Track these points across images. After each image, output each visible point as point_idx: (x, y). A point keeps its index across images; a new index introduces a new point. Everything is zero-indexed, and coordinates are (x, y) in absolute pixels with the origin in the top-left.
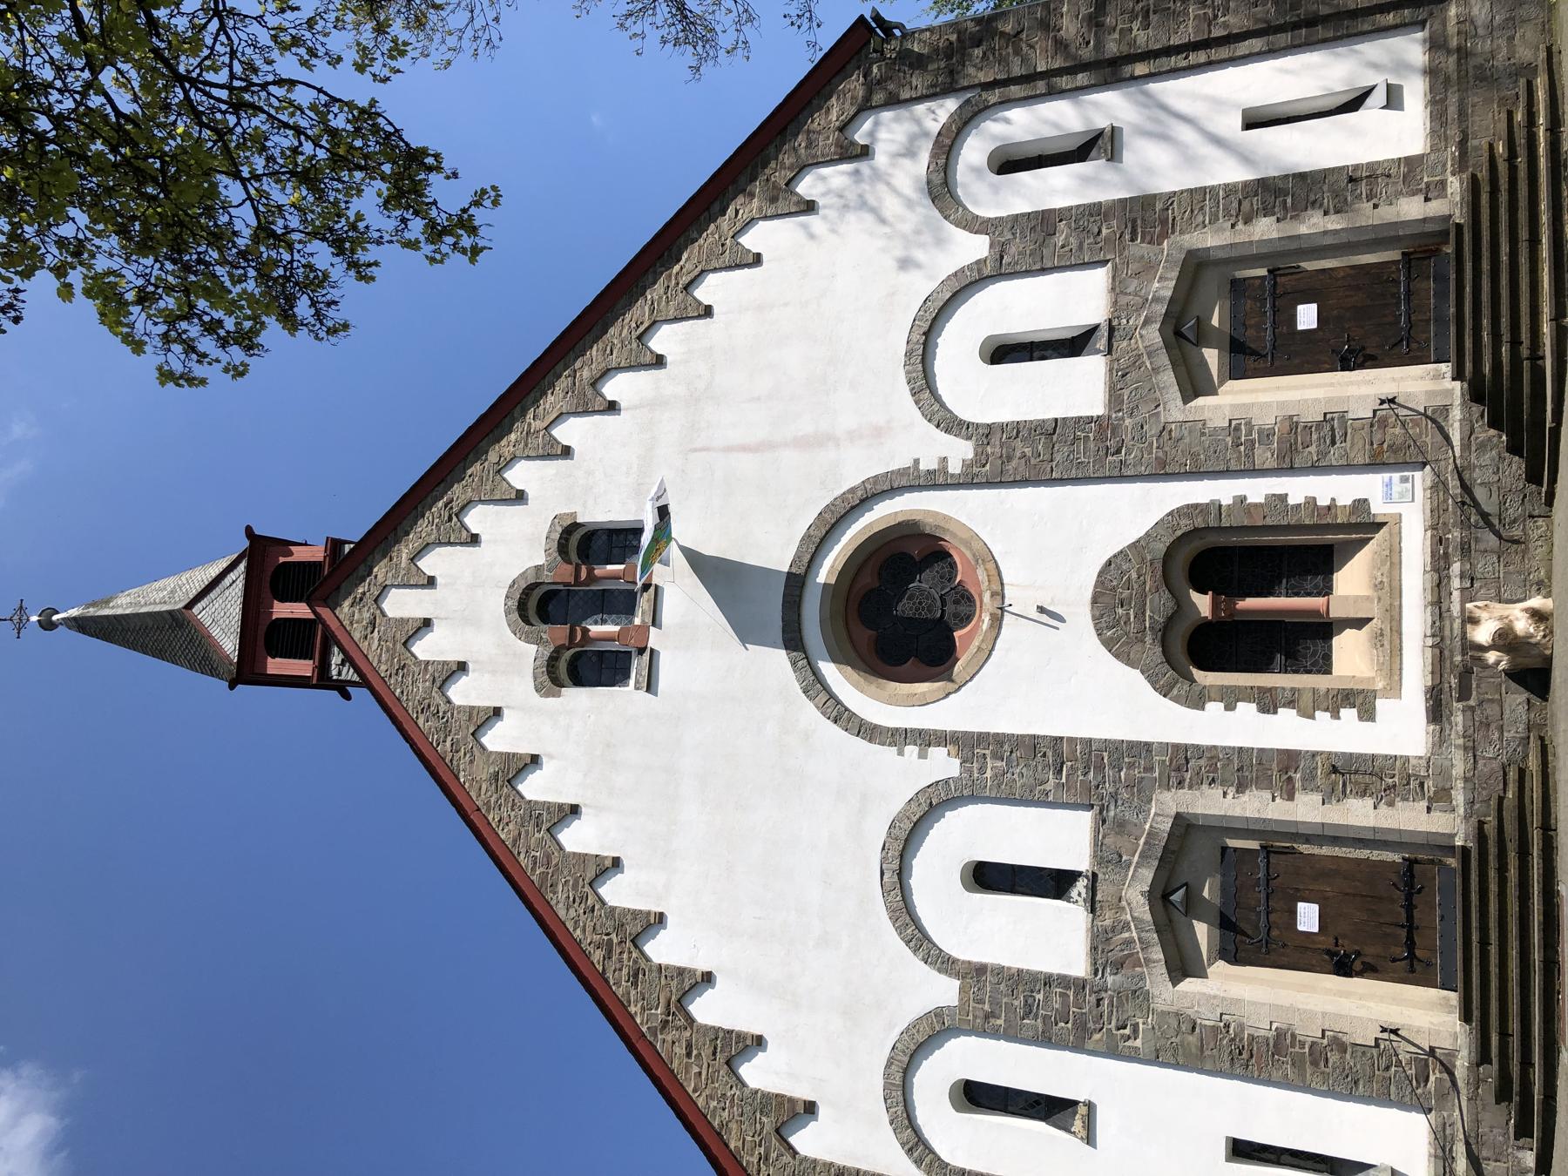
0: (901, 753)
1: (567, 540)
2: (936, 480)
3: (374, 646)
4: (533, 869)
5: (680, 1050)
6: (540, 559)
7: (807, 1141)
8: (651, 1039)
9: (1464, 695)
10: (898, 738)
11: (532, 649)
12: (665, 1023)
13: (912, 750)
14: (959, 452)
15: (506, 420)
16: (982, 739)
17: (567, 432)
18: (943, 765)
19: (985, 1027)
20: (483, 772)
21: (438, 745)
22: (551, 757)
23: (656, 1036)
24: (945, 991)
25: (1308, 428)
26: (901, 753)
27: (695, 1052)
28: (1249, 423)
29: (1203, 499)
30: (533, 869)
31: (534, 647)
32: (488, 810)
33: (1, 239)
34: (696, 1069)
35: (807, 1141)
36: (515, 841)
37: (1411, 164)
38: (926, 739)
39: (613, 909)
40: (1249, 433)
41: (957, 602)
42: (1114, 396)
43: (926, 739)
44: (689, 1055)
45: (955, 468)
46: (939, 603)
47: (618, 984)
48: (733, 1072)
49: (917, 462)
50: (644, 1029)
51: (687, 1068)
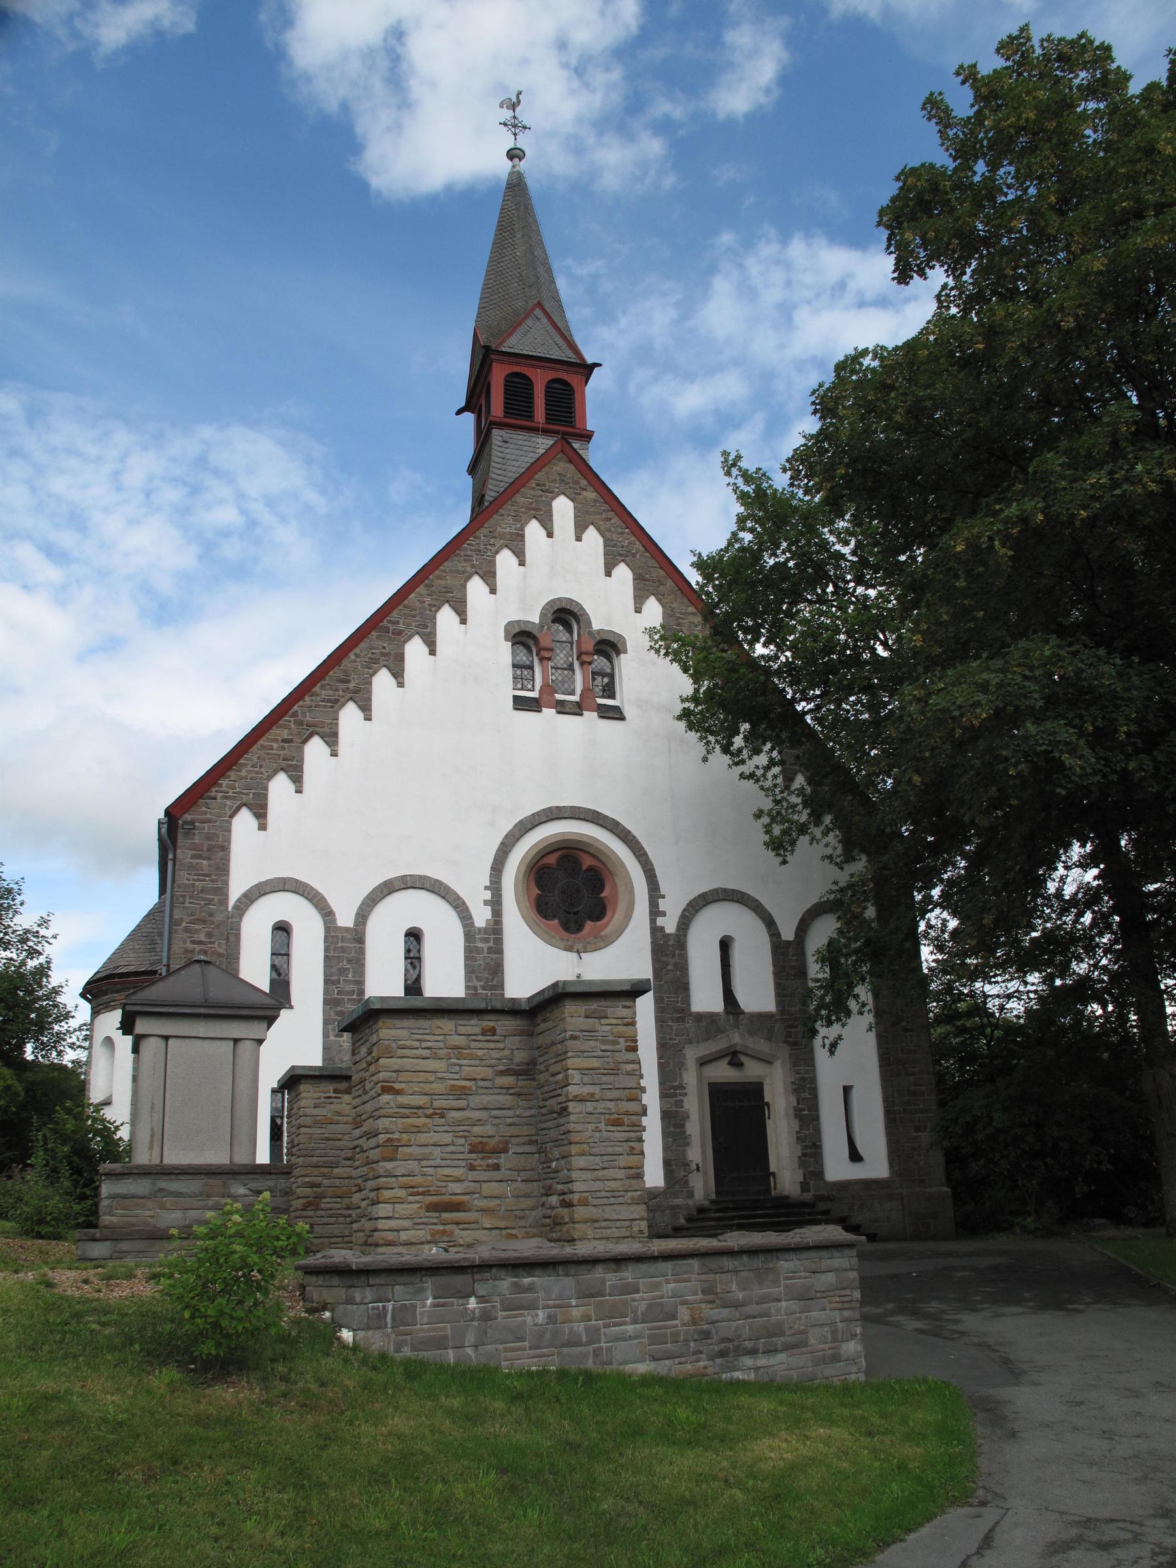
0: (486, 888)
1: (607, 644)
2: (655, 912)
3: (532, 492)
4: (390, 622)
5: (285, 734)
6: (596, 626)
7: (244, 822)
8: (290, 713)
9: (544, 485)
10: (495, 886)
11: (536, 620)
12: (301, 723)
13: (488, 895)
14: (669, 924)
15: (686, 601)
16: (499, 941)
17: (623, 573)
18: (481, 917)
19: (332, 934)
20: (450, 581)
21: (468, 544)
22: (466, 633)
23: (292, 716)
24: (345, 919)
25: (683, 1126)
26: (486, 888)
27: (286, 745)
28: (686, 1094)
29: (644, 1070)
30: (390, 622)
31: (537, 621)
32: (426, 586)
33: (1, 1103)
34: (275, 746)
35: (244, 822)
36: (406, 607)
37: (819, 1174)
38: (496, 903)
39: (370, 683)
40: (681, 1095)
41: (576, 922)
42: (700, 1017)
43: (496, 903)
44: (284, 741)
45: (660, 921)
46: (575, 910)
47: (322, 688)
48: (375, 661)
49: (663, 897)
50: (295, 708)
51: (276, 741)
